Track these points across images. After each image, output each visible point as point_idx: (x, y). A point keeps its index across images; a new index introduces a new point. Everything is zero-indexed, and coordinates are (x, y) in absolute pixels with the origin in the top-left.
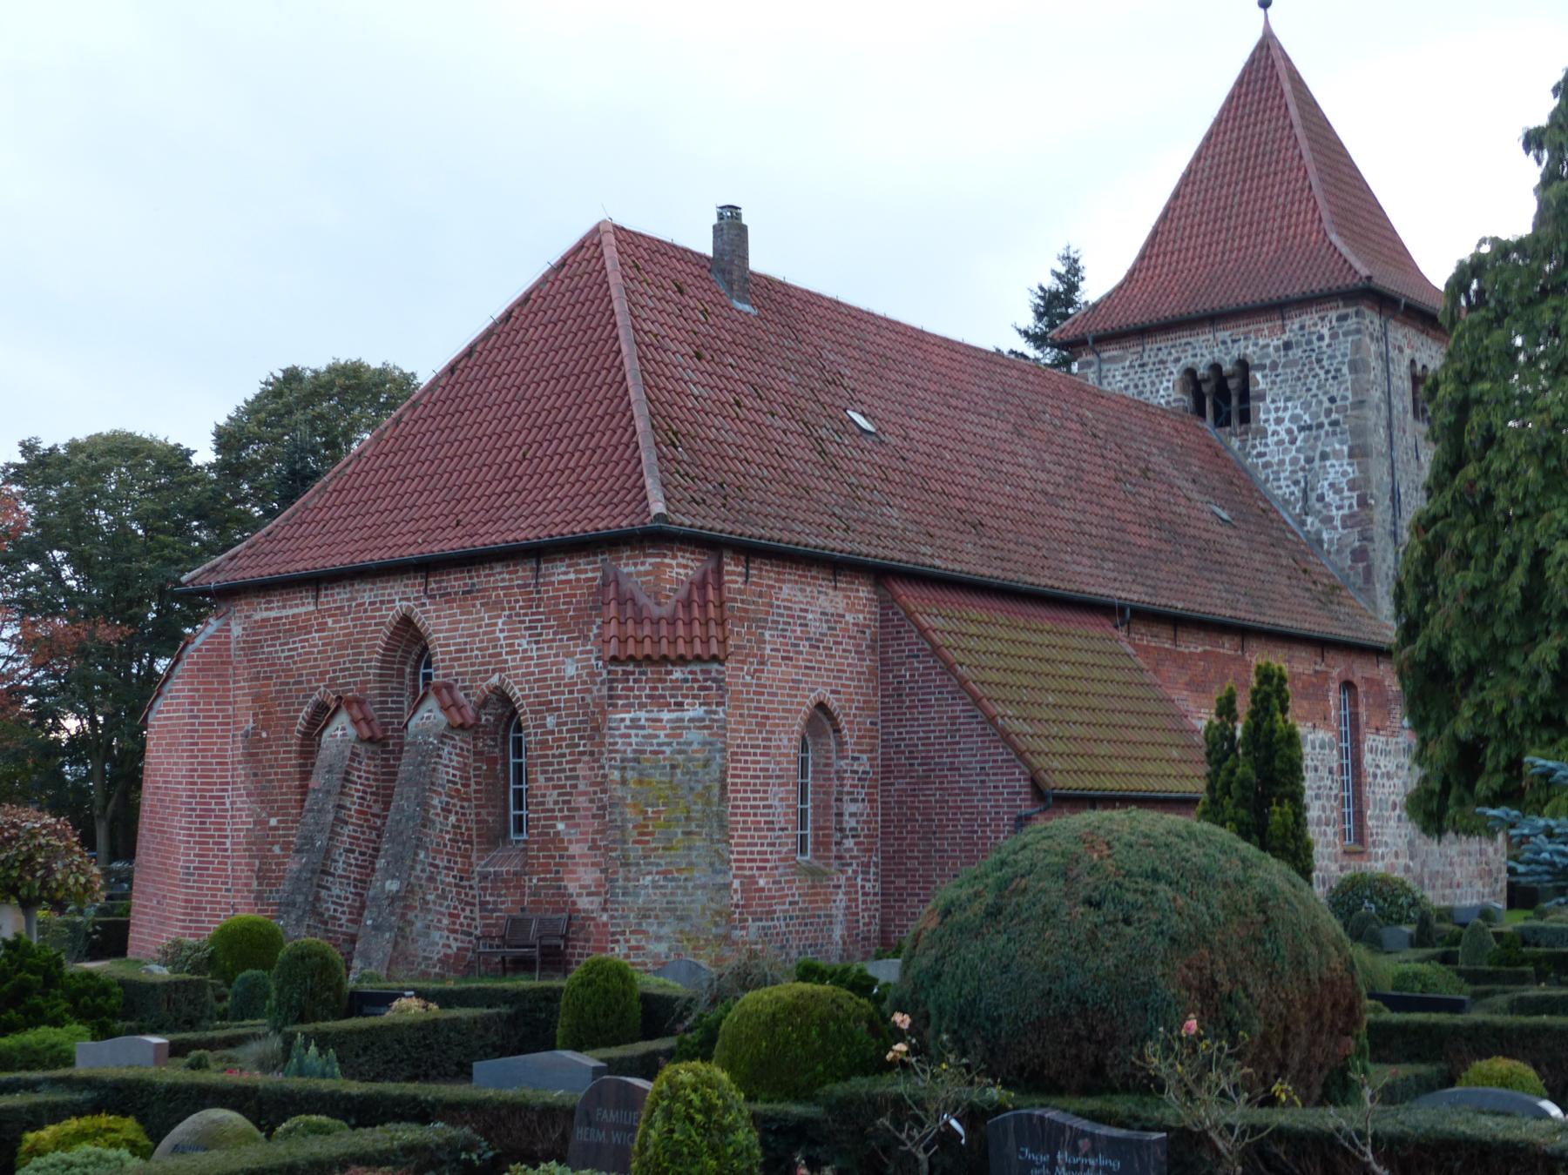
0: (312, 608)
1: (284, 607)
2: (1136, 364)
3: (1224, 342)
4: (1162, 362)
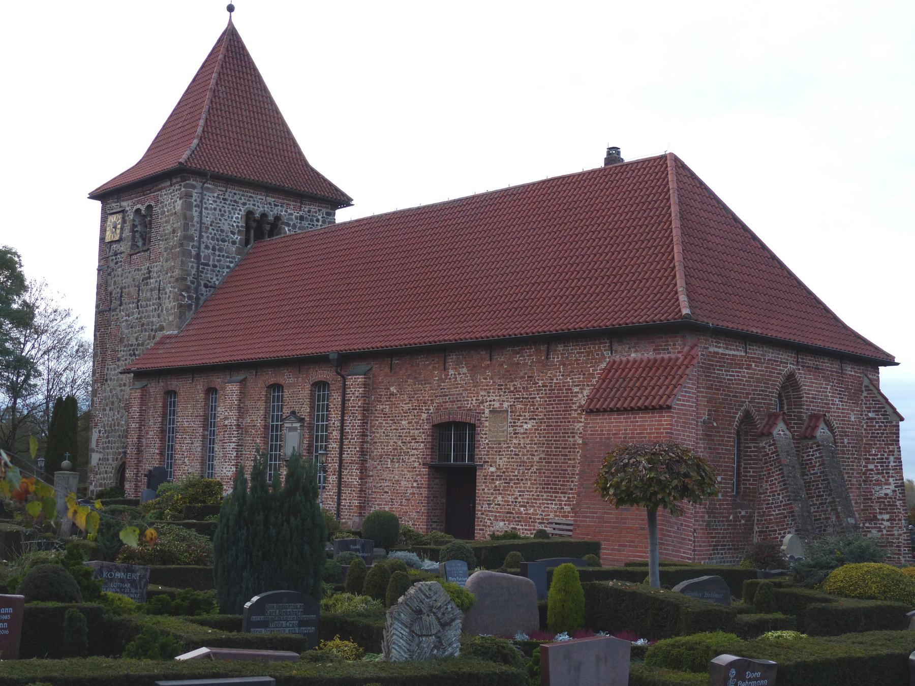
0: (743, 354)
1: (727, 348)
2: (222, 197)
3: (270, 204)
4: (235, 201)
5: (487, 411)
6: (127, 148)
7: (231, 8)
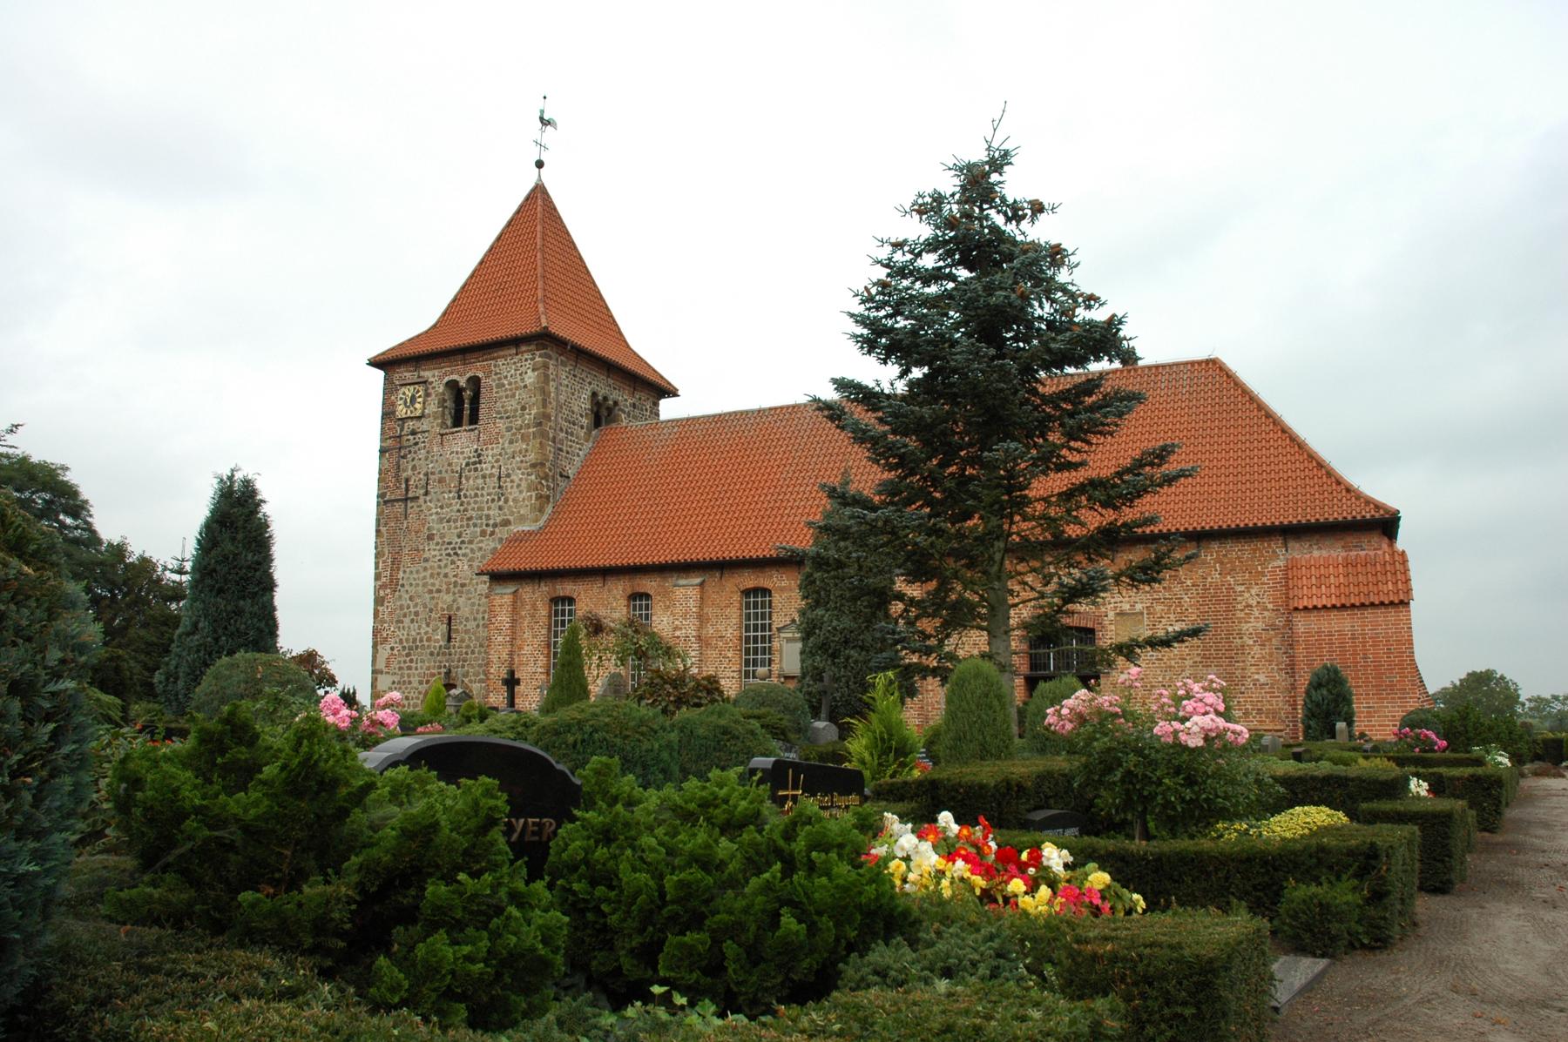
5: (1111, 615)
6: (416, 313)
7: (540, 164)
